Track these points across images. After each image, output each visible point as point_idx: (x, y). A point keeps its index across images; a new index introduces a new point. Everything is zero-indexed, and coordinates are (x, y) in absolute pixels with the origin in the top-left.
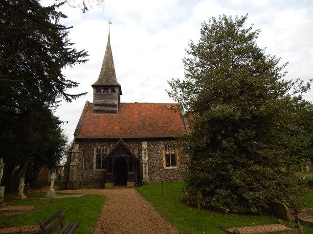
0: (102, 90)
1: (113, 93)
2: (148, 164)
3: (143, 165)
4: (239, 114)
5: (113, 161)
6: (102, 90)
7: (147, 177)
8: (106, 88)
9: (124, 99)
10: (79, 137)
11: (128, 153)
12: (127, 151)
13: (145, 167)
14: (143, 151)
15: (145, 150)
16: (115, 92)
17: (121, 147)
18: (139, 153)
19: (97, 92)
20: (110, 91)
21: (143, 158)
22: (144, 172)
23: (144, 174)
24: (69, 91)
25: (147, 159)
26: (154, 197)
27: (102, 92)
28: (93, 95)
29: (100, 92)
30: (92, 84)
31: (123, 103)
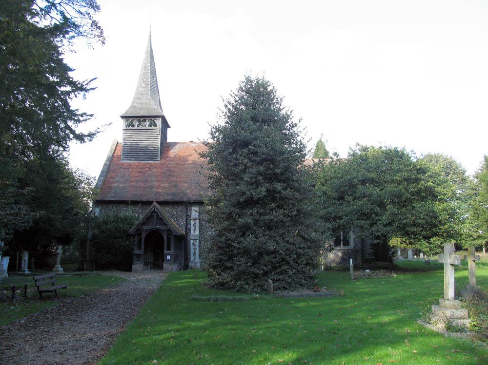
0: (136, 123)
1: (153, 127)
2: (200, 242)
3: (192, 242)
4: (418, 341)
5: (144, 235)
6: (136, 123)
7: (197, 260)
8: (142, 118)
9: (71, 109)
10: (99, 198)
11: (165, 224)
12: (160, 220)
13: (194, 244)
14: (192, 222)
15: (195, 219)
16: (156, 125)
17: (155, 215)
18: (187, 223)
19: (129, 126)
20: (147, 123)
21: (192, 231)
22: (192, 251)
23: (192, 255)
24: (80, 129)
25: (197, 232)
26: (82, 330)
27: (136, 126)
28: (122, 131)
29: (133, 126)
30: (123, 112)
31: (170, 143)
